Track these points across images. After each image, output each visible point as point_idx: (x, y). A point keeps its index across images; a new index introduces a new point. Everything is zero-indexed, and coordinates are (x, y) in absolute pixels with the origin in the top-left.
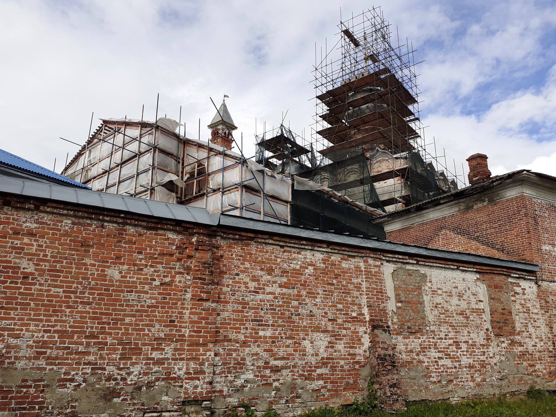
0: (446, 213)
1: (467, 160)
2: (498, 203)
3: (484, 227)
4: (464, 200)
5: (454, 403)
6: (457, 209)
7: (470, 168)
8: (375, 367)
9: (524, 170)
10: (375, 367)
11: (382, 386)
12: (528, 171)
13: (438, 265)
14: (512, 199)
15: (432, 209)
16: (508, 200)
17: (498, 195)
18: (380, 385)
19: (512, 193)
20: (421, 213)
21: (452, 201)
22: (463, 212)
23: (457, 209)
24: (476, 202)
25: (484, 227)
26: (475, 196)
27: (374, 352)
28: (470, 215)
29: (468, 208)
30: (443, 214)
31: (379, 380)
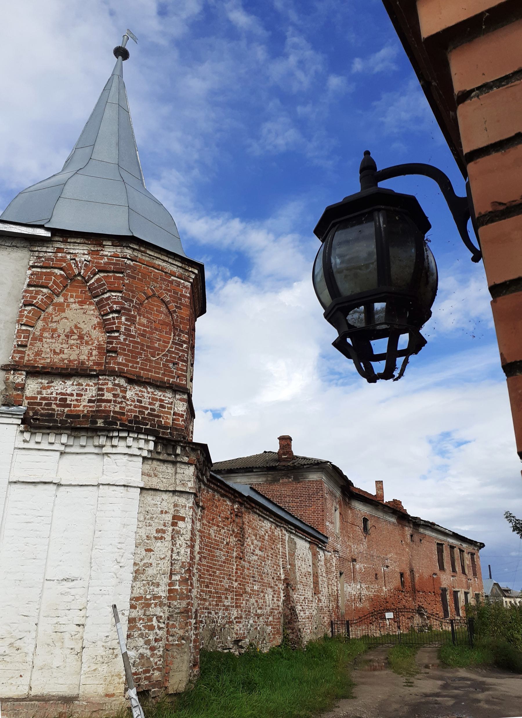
0: (254, 480)
1: (278, 438)
2: (302, 482)
3: (287, 499)
4: (273, 473)
5: (265, 651)
6: (264, 479)
7: (280, 446)
8: (288, 616)
9: (329, 462)
10: (288, 616)
11: (294, 630)
12: (330, 463)
13: (300, 535)
14: (313, 481)
15: (241, 474)
16: (309, 481)
17: (302, 475)
18: (293, 630)
19: (314, 477)
20: (229, 475)
21: (263, 471)
22: (269, 483)
23: (264, 479)
24: (282, 477)
25: (287, 499)
26: (283, 472)
27: (288, 604)
28: (276, 487)
29: (275, 481)
30: (250, 480)
31: (291, 626)
